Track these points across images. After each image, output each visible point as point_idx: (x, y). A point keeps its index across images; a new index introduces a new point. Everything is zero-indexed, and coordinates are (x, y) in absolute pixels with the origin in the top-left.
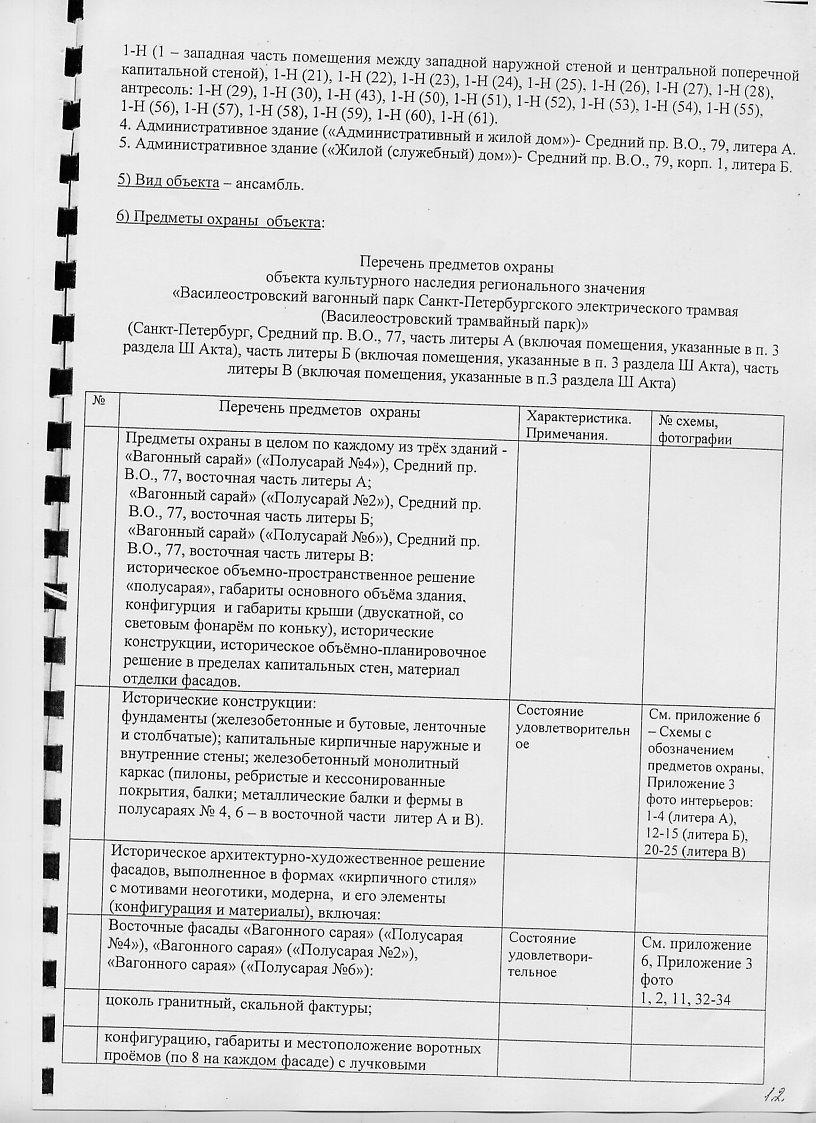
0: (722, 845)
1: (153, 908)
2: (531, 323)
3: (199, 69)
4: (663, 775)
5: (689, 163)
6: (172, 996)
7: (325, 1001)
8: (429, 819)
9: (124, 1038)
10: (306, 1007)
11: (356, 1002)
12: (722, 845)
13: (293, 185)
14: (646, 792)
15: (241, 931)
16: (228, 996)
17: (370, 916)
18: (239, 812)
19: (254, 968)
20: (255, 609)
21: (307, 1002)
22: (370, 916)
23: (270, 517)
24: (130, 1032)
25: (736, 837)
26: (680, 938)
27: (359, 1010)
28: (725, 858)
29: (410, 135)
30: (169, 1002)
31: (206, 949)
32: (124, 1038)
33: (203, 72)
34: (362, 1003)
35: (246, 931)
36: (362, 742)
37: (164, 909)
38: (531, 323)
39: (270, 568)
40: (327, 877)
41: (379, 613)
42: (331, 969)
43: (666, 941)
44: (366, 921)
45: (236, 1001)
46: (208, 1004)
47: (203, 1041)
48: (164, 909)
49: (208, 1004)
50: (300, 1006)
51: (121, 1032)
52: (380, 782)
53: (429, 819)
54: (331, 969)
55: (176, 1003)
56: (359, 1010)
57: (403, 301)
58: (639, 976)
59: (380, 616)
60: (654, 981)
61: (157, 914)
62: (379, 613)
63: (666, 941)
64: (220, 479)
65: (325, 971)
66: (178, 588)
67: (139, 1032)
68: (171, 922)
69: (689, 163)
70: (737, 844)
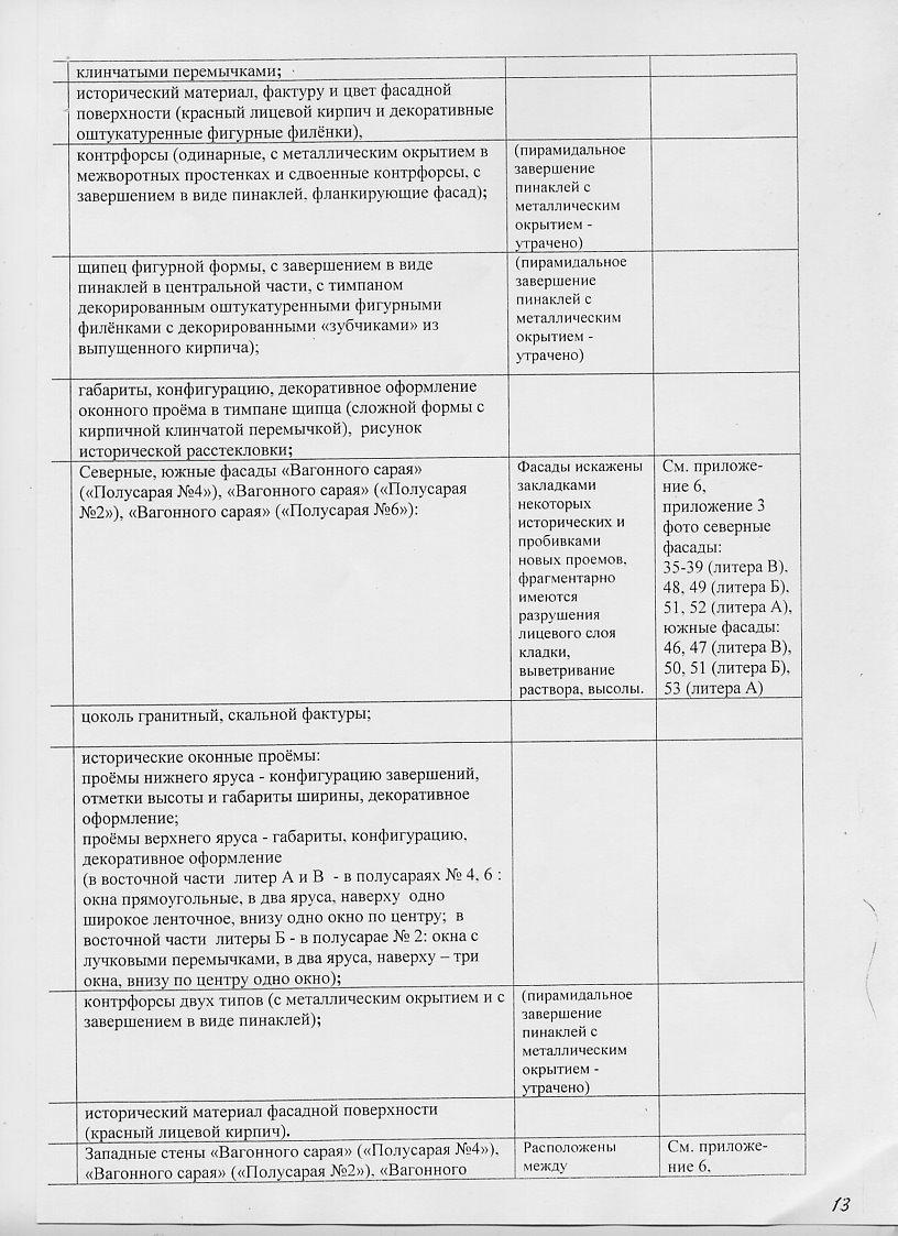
0: (759, 659)
1: (223, 134)
2: (210, 715)
3: (169, 875)
4: (681, 518)
5: (398, 796)
6: (153, 710)
7: (320, 708)
8: (273, 878)
9: (177, 391)
10: (299, 715)
11: (353, 707)
12: (759, 659)
13: (201, 899)
14: (662, 518)
15: (279, 472)
16: (214, 707)
17: (318, 1173)
18: (317, 195)
19: (290, 512)
20: (242, 798)
21: (300, 709)
22: (318, 1173)
23: (170, 940)
24: (184, 384)
25: (775, 589)
26: (708, 1141)
27: (356, 715)
28: (738, 695)
29: (204, 288)
30: (150, 716)
31: (209, 922)
32: (177, 391)
33: (216, 1132)
34: (360, 708)
35: (285, 472)
36: (124, 431)
37: (235, 135)
38: (210, 715)
39: (177, 519)
40: (262, 175)
41: (197, 1001)
42: (372, 510)
43: (694, 1144)
44: (315, 1178)
45: (223, 712)
46: (193, 717)
47: (265, 390)
48: (235, 135)
49: (193, 717)
50: (292, 715)
51: (173, 384)
52: (231, 330)
53: (273, 878)
54: (372, 510)
55: (160, 718)
56: (356, 715)
57: (115, 391)
58: (661, 523)
59: (199, 1005)
60: (678, 528)
61: (228, 140)
62: (197, 1001)
63: (694, 1144)
64: (191, 920)
65: (366, 511)
66: (745, 648)
67: (194, 384)
68: (247, 148)
69: (398, 796)
70: (777, 596)
